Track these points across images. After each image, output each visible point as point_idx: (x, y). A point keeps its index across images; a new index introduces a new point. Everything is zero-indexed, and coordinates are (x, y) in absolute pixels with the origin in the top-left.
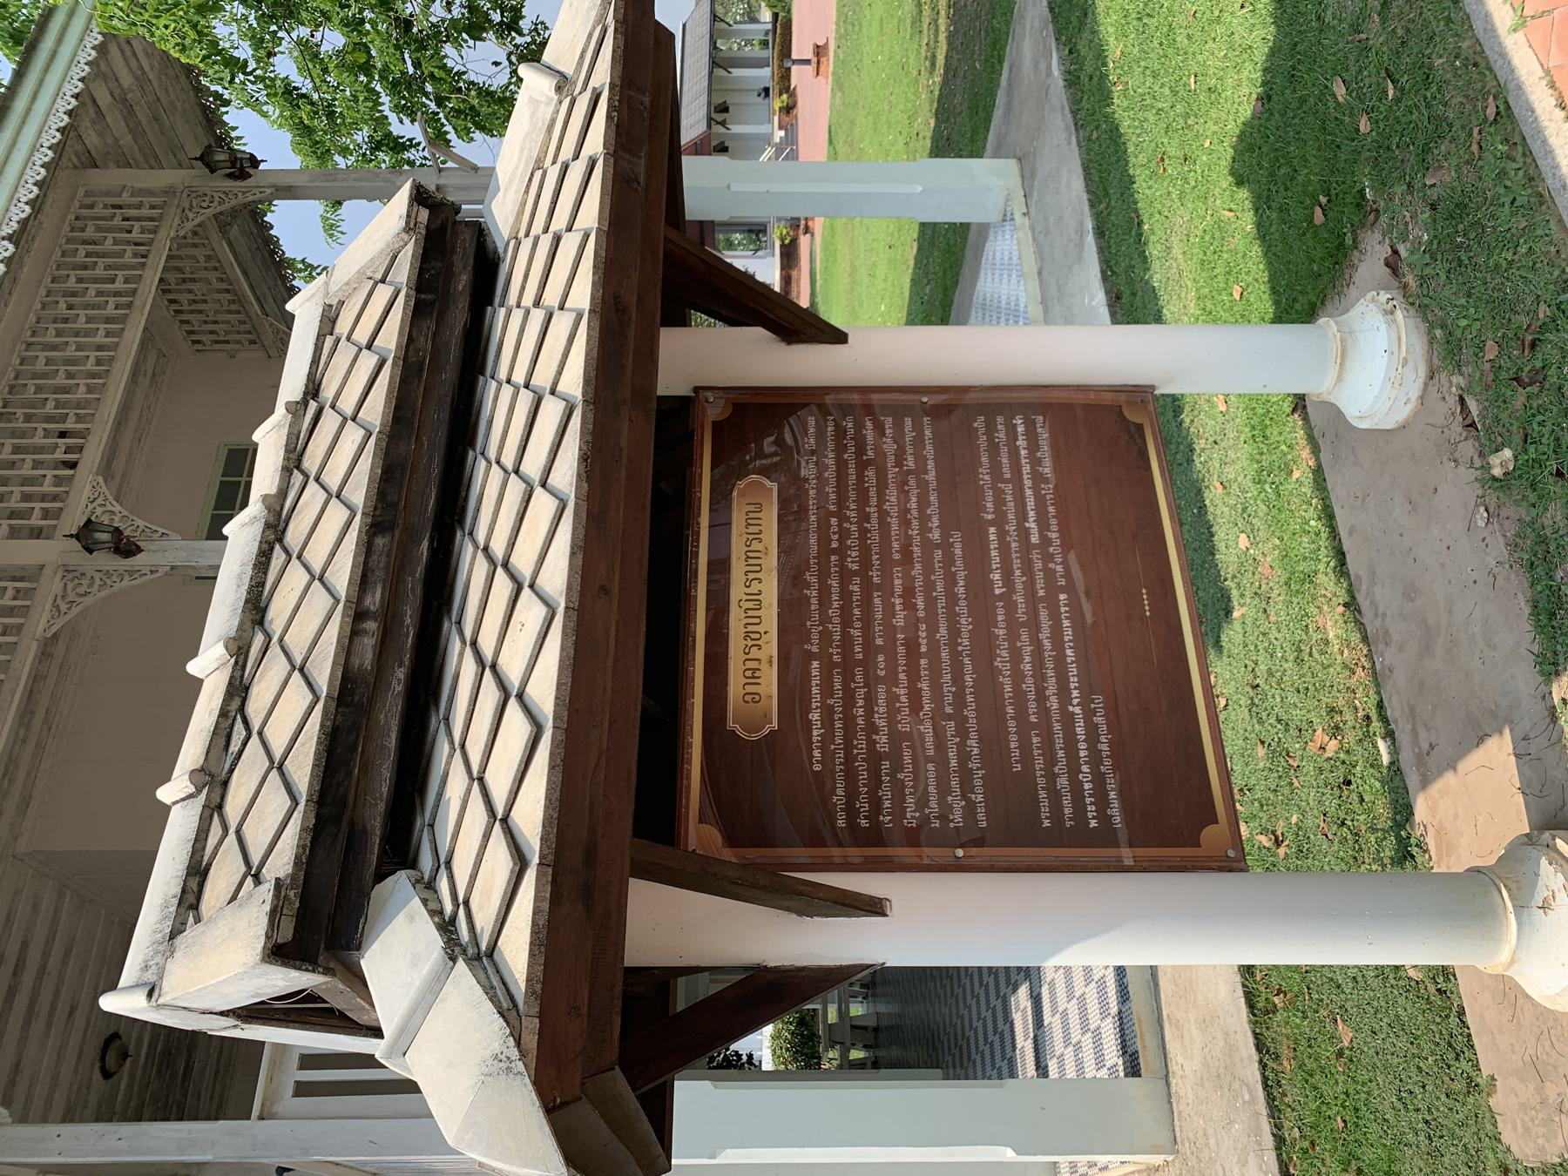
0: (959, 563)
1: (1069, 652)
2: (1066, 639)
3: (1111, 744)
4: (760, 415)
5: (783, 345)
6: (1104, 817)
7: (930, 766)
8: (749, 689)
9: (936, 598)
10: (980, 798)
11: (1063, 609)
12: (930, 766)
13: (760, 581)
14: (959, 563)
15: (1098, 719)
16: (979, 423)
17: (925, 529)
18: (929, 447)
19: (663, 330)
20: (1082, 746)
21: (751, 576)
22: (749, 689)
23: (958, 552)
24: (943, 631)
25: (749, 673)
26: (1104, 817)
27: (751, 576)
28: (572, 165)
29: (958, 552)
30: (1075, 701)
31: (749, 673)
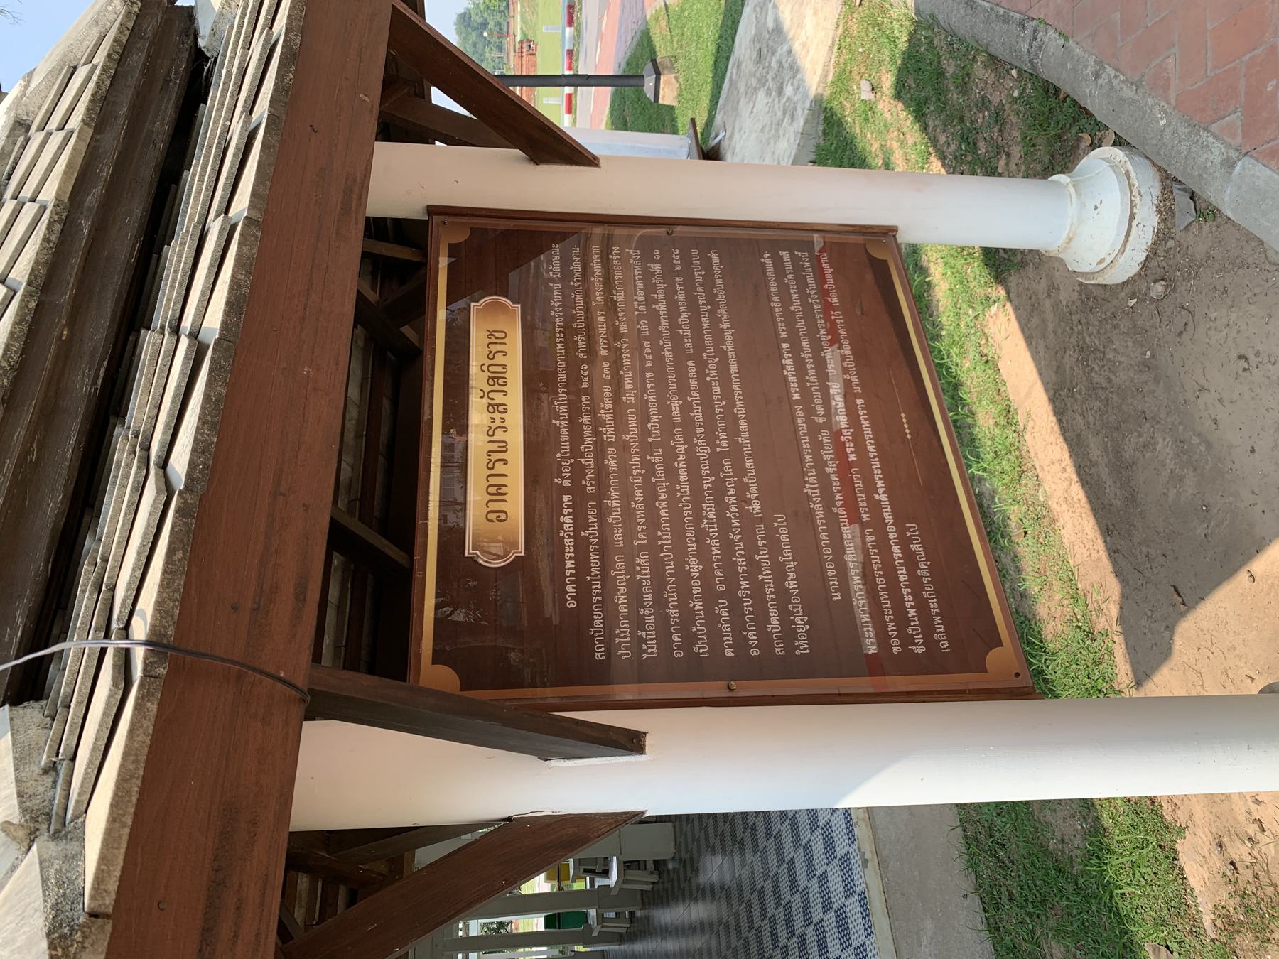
0: (787, 552)
1: (870, 448)
2: (867, 437)
3: (930, 568)
4: (503, 249)
5: (532, 167)
6: (930, 643)
7: (690, 363)
8: (493, 506)
9: (762, 582)
10: (730, 348)
11: (861, 412)
12: (690, 363)
13: (505, 462)
14: (787, 552)
15: (915, 546)
16: (766, 259)
17: (743, 501)
18: (739, 405)
19: (377, 144)
20: (896, 549)
21: (494, 456)
22: (493, 506)
23: (784, 538)
24: (774, 621)
25: (493, 490)
26: (930, 643)
27: (494, 456)
28: (28, 204)
29: (784, 538)
30: (881, 491)
31: (493, 490)
